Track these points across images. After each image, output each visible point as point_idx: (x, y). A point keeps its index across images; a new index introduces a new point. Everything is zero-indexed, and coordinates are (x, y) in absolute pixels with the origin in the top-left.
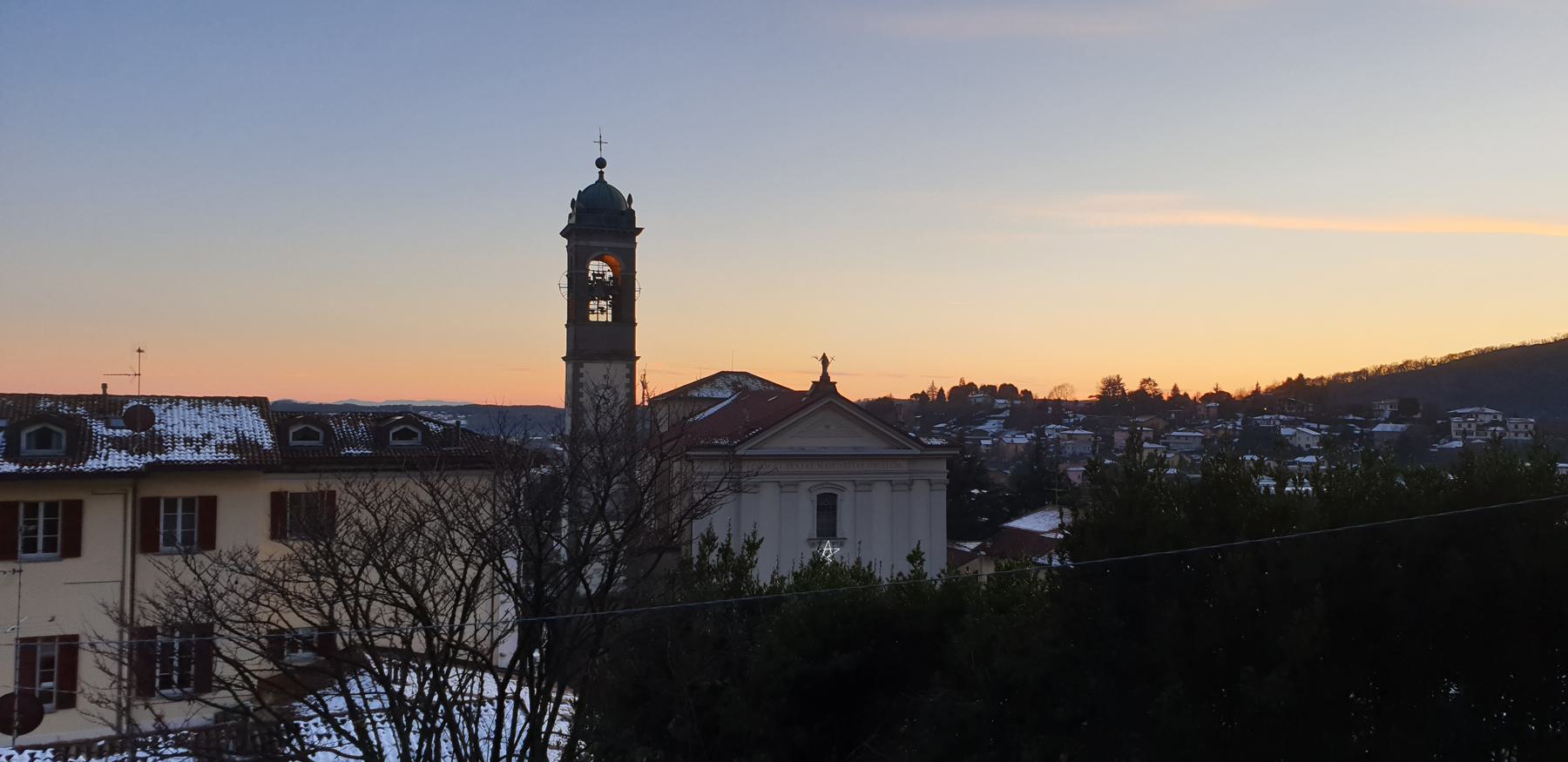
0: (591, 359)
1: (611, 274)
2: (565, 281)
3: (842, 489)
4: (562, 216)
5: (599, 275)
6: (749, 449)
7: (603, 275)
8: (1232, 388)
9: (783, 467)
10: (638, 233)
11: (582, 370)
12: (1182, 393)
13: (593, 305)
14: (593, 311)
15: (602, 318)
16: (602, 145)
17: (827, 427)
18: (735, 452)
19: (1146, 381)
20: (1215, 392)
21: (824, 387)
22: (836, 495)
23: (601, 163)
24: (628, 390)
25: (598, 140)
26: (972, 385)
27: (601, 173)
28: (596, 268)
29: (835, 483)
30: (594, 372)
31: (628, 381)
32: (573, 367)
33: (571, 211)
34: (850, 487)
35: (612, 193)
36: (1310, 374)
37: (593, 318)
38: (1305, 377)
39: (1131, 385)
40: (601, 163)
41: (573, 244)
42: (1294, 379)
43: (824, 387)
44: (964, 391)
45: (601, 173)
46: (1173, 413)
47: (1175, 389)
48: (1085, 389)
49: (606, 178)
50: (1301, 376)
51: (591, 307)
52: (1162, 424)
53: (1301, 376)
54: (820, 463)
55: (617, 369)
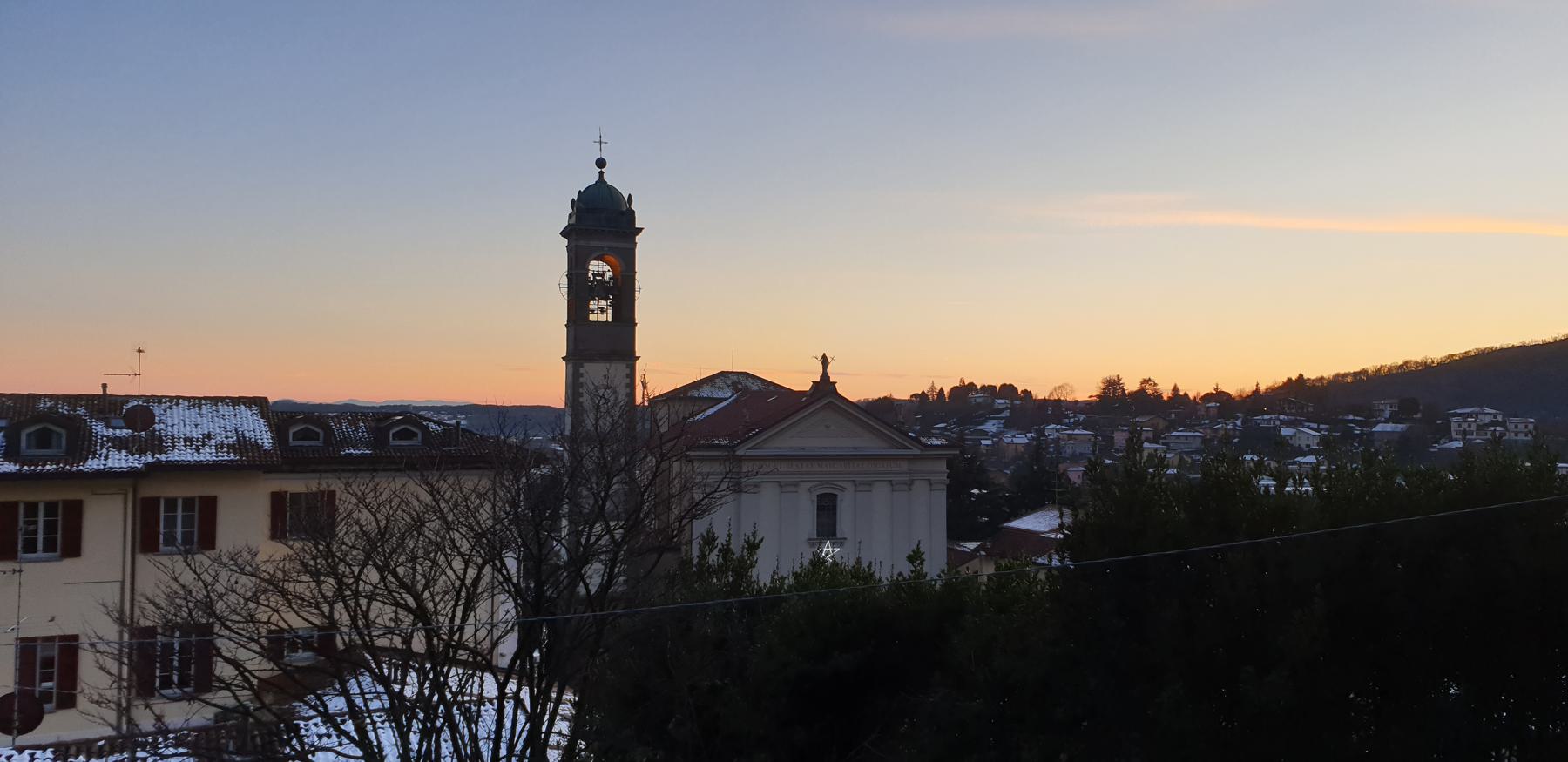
0: (591, 359)
1: (611, 274)
2: (565, 281)
3: (842, 489)
4: (562, 216)
5: (599, 275)
6: (749, 449)
7: (603, 275)
8: (1232, 388)
9: (783, 467)
10: (638, 233)
11: (582, 370)
12: (1182, 393)
13: (593, 305)
14: (593, 311)
15: (602, 318)
16: (602, 145)
17: (827, 427)
18: (735, 452)
19: (1146, 381)
20: (1215, 392)
21: (824, 387)
22: (836, 495)
23: (601, 163)
24: (628, 390)
25: (598, 140)
26: (972, 385)
27: (601, 173)
28: (596, 268)
29: (835, 483)
30: (594, 372)
31: (628, 381)
32: (573, 367)
33: (571, 211)
34: (850, 487)
35: (612, 193)
36: (1310, 374)
37: (593, 318)
38: (1305, 377)
39: (1131, 385)
40: (601, 163)
41: (573, 244)
42: (1294, 379)
43: (824, 387)
44: (964, 391)
45: (601, 173)
46: (1173, 413)
47: (1175, 389)
48: (1085, 389)
49: (606, 178)
50: (1301, 376)
51: (591, 307)
52: (1162, 424)
53: (1301, 376)
54: (820, 463)
55: (617, 369)
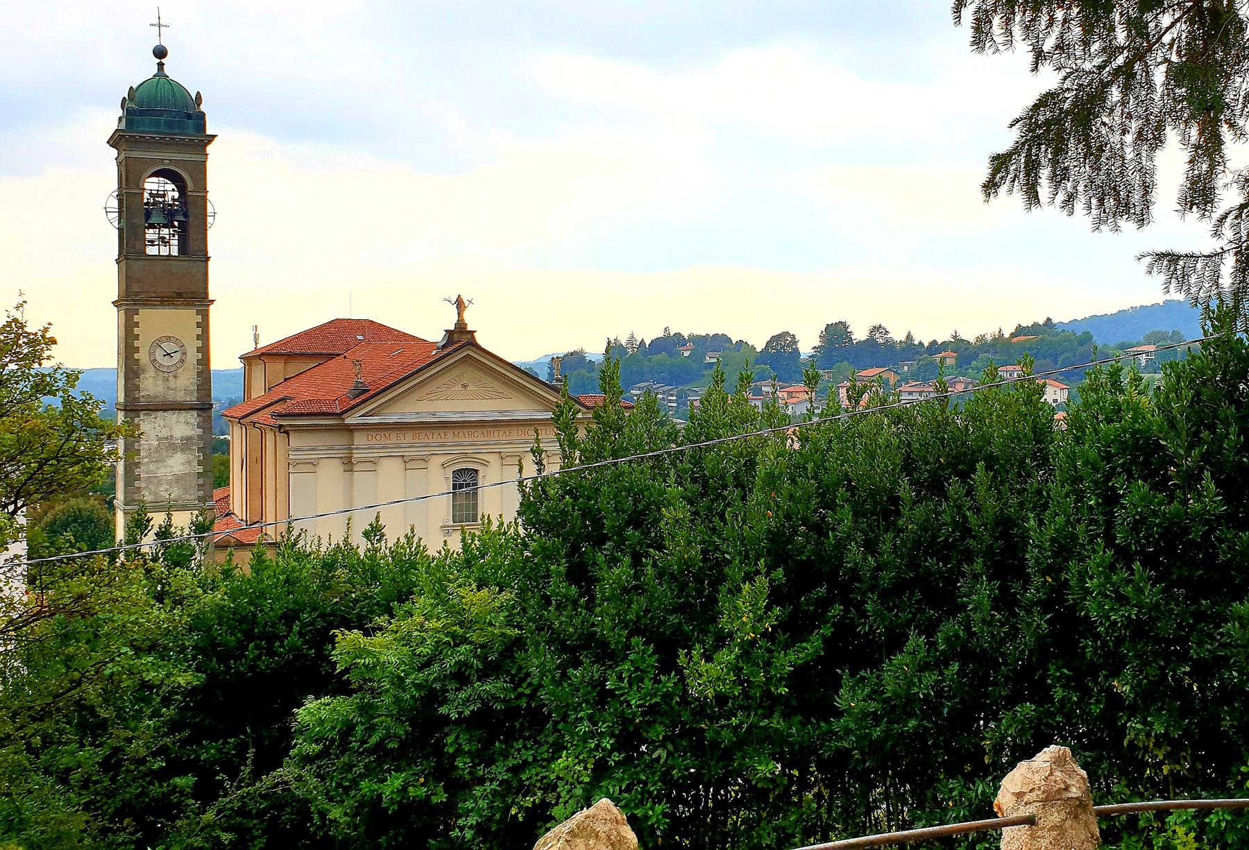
0: (148, 303)
1: (176, 195)
2: (114, 203)
3: (486, 464)
4: (110, 119)
5: (158, 195)
6: (363, 416)
7: (163, 196)
8: (970, 336)
9: (408, 438)
10: (210, 142)
11: (136, 318)
12: (916, 342)
13: (151, 234)
14: (152, 241)
15: (164, 251)
16: (162, 28)
17: (465, 386)
18: (343, 420)
19: (876, 329)
20: (953, 340)
21: (460, 338)
22: (476, 471)
23: (160, 53)
24: (199, 344)
25: (156, 22)
26: (678, 335)
27: (161, 65)
28: (155, 187)
29: (475, 456)
30: (154, 321)
31: (199, 331)
32: (126, 314)
33: (203, 108)
34: (493, 459)
35: (177, 90)
36: (1061, 316)
37: (151, 251)
38: (1055, 321)
39: (860, 333)
40: (160, 53)
41: (123, 156)
42: (1041, 323)
43: (460, 338)
44: (669, 343)
45: (161, 65)
46: (907, 365)
47: (909, 337)
48: (595, 350)
49: (167, 70)
50: (1049, 319)
51: (148, 237)
52: (893, 378)
53: (1049, 319)
54: (523, 429)
55: (186, 317)
